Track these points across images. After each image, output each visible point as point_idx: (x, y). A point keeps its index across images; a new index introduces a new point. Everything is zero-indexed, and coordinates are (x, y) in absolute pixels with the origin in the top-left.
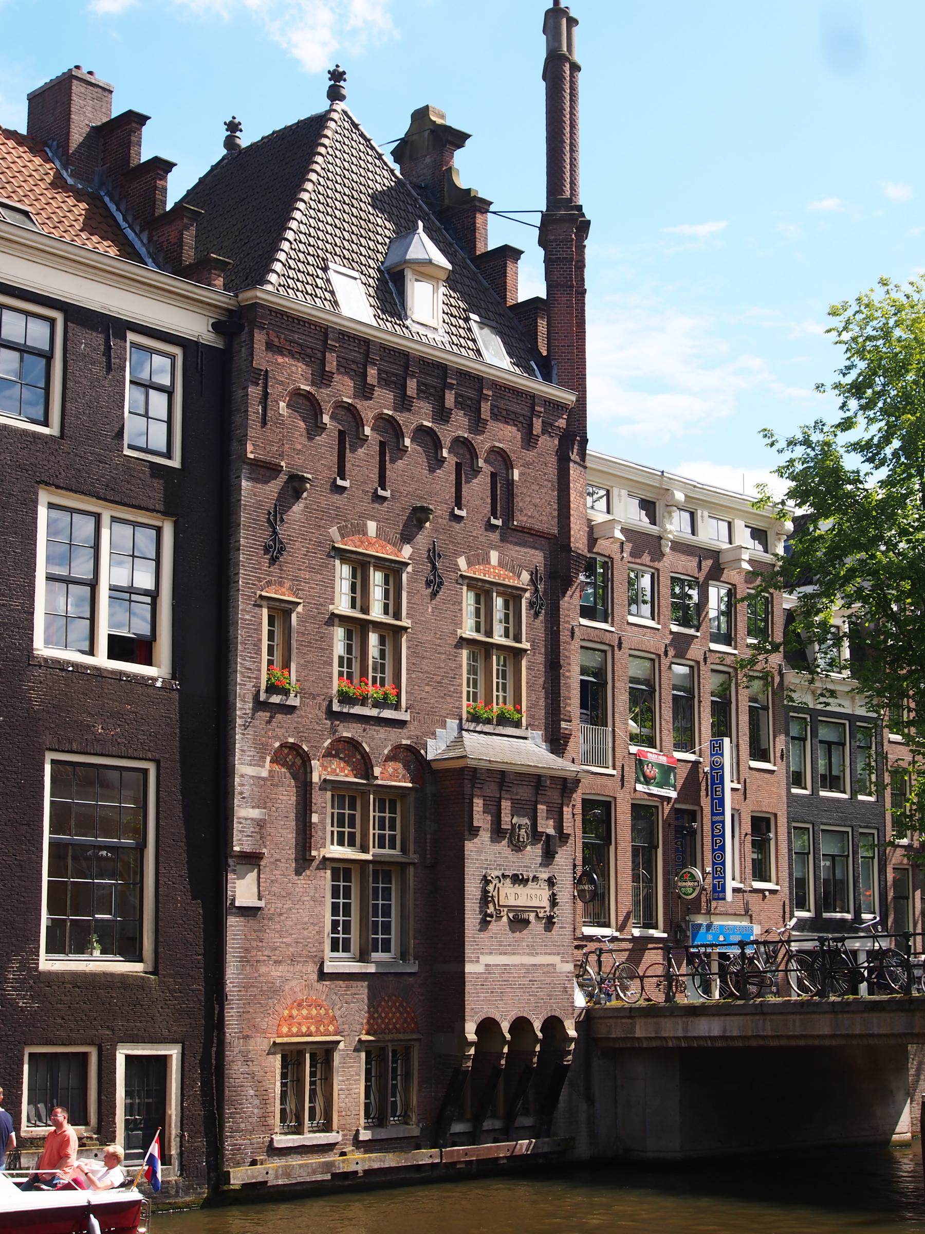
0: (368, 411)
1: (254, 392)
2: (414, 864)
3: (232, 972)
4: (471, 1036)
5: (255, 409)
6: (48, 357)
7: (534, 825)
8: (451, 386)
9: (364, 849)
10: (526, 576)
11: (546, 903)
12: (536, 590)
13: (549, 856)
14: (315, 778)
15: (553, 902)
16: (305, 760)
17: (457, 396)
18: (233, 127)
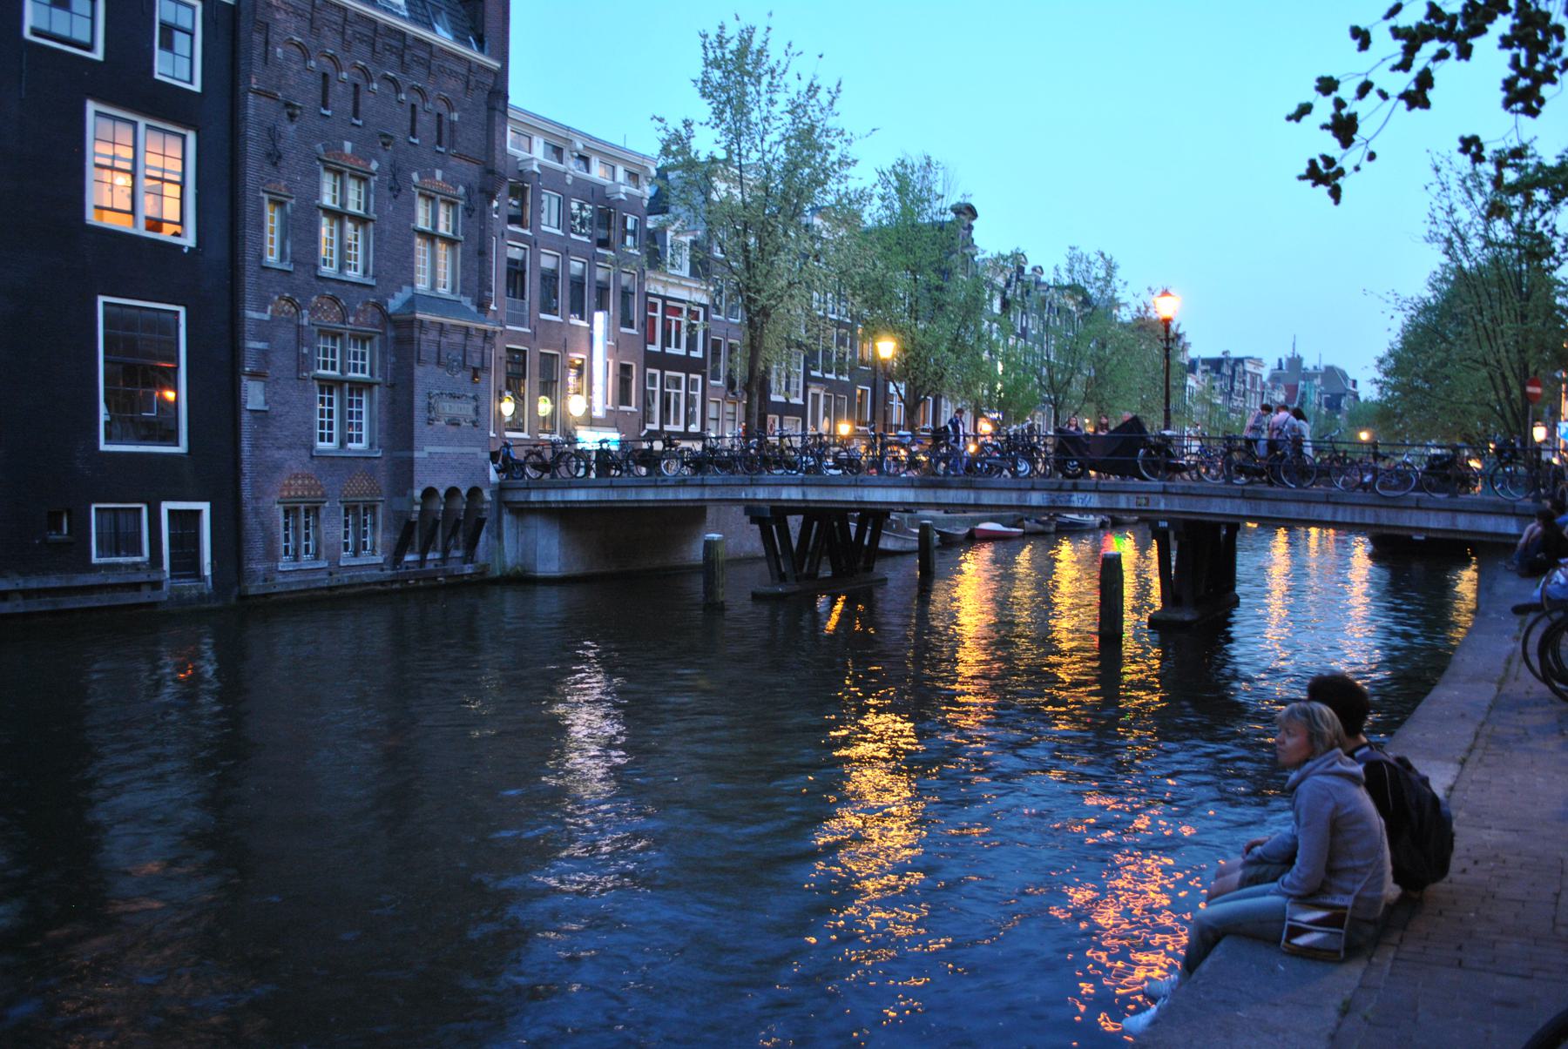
1: (258, 38)
2: (379, 384)
5: (258, 52)
10: (461, 189)
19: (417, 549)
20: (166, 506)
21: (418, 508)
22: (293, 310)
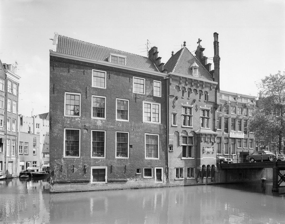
0: (187, 87)
3: (169, 159)
4: (201, 167)
6: (160, 88)
7: (211, 141)
8: (199, 83)
9: (187, 144)
10: (210, 108)
11: (212, 151)
12: (212, 110)
13: (213, 144)
14: (180, 135)
15: (213, 150)
16: (179, 133)
17: (194, 83)
18: (173, 52)
19: (211, 176)
20: (156, 168)
21: (201, 169)
22: (178, 133)
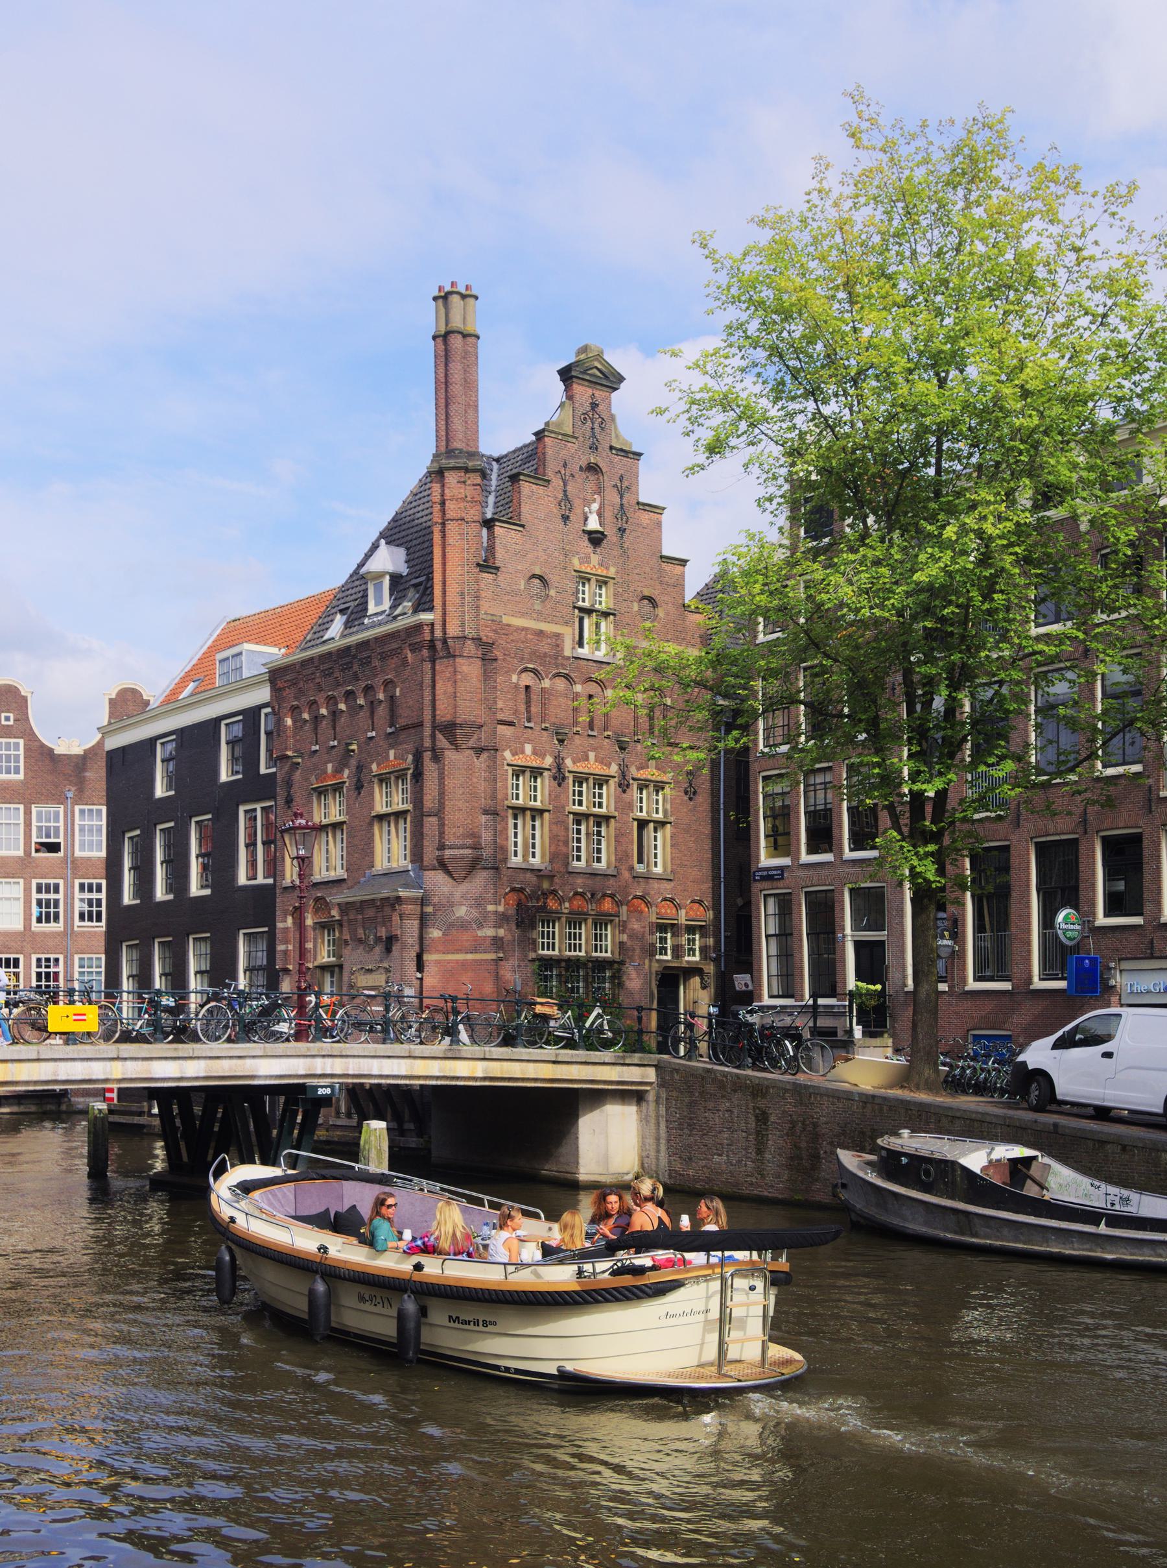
10: (410, 758)
